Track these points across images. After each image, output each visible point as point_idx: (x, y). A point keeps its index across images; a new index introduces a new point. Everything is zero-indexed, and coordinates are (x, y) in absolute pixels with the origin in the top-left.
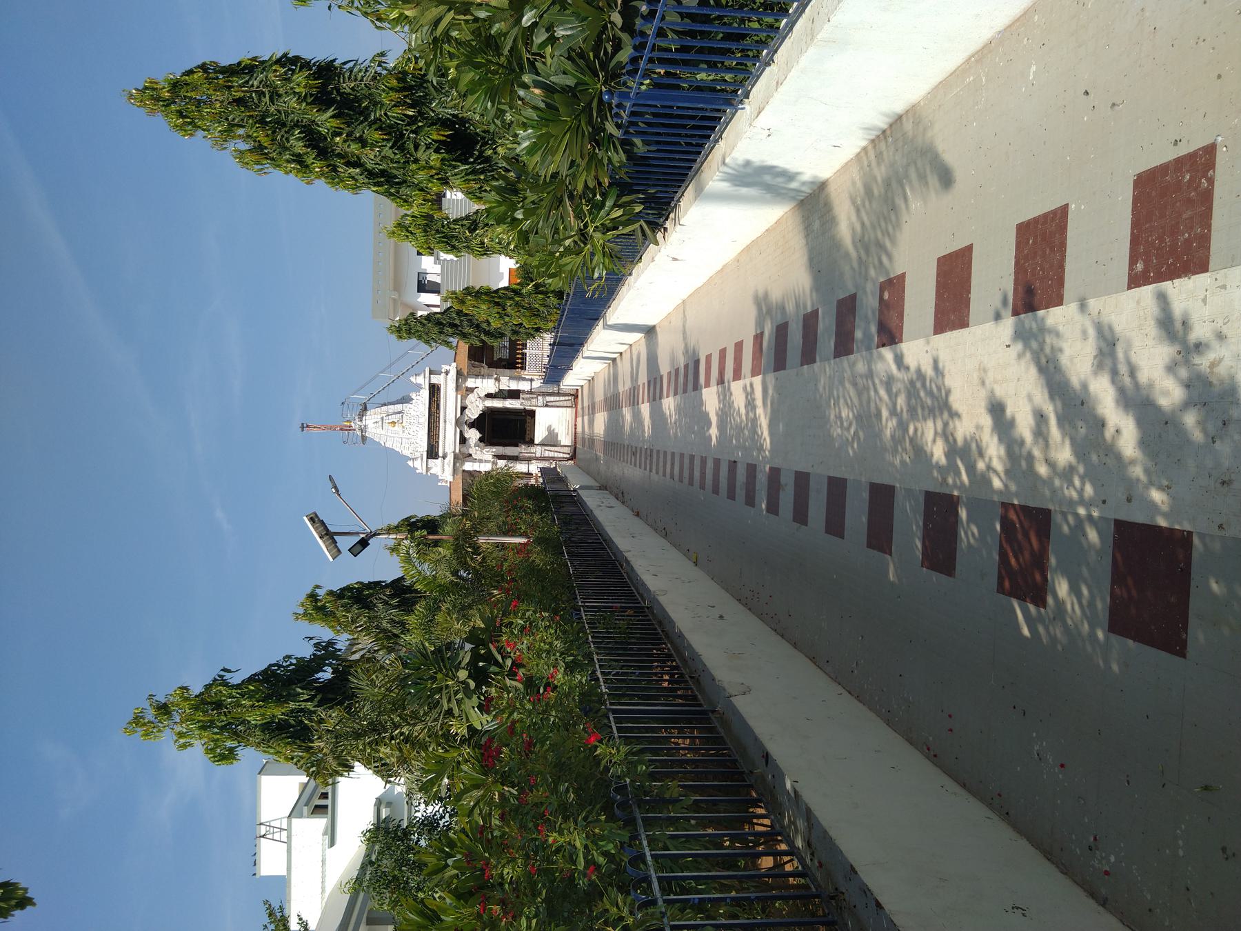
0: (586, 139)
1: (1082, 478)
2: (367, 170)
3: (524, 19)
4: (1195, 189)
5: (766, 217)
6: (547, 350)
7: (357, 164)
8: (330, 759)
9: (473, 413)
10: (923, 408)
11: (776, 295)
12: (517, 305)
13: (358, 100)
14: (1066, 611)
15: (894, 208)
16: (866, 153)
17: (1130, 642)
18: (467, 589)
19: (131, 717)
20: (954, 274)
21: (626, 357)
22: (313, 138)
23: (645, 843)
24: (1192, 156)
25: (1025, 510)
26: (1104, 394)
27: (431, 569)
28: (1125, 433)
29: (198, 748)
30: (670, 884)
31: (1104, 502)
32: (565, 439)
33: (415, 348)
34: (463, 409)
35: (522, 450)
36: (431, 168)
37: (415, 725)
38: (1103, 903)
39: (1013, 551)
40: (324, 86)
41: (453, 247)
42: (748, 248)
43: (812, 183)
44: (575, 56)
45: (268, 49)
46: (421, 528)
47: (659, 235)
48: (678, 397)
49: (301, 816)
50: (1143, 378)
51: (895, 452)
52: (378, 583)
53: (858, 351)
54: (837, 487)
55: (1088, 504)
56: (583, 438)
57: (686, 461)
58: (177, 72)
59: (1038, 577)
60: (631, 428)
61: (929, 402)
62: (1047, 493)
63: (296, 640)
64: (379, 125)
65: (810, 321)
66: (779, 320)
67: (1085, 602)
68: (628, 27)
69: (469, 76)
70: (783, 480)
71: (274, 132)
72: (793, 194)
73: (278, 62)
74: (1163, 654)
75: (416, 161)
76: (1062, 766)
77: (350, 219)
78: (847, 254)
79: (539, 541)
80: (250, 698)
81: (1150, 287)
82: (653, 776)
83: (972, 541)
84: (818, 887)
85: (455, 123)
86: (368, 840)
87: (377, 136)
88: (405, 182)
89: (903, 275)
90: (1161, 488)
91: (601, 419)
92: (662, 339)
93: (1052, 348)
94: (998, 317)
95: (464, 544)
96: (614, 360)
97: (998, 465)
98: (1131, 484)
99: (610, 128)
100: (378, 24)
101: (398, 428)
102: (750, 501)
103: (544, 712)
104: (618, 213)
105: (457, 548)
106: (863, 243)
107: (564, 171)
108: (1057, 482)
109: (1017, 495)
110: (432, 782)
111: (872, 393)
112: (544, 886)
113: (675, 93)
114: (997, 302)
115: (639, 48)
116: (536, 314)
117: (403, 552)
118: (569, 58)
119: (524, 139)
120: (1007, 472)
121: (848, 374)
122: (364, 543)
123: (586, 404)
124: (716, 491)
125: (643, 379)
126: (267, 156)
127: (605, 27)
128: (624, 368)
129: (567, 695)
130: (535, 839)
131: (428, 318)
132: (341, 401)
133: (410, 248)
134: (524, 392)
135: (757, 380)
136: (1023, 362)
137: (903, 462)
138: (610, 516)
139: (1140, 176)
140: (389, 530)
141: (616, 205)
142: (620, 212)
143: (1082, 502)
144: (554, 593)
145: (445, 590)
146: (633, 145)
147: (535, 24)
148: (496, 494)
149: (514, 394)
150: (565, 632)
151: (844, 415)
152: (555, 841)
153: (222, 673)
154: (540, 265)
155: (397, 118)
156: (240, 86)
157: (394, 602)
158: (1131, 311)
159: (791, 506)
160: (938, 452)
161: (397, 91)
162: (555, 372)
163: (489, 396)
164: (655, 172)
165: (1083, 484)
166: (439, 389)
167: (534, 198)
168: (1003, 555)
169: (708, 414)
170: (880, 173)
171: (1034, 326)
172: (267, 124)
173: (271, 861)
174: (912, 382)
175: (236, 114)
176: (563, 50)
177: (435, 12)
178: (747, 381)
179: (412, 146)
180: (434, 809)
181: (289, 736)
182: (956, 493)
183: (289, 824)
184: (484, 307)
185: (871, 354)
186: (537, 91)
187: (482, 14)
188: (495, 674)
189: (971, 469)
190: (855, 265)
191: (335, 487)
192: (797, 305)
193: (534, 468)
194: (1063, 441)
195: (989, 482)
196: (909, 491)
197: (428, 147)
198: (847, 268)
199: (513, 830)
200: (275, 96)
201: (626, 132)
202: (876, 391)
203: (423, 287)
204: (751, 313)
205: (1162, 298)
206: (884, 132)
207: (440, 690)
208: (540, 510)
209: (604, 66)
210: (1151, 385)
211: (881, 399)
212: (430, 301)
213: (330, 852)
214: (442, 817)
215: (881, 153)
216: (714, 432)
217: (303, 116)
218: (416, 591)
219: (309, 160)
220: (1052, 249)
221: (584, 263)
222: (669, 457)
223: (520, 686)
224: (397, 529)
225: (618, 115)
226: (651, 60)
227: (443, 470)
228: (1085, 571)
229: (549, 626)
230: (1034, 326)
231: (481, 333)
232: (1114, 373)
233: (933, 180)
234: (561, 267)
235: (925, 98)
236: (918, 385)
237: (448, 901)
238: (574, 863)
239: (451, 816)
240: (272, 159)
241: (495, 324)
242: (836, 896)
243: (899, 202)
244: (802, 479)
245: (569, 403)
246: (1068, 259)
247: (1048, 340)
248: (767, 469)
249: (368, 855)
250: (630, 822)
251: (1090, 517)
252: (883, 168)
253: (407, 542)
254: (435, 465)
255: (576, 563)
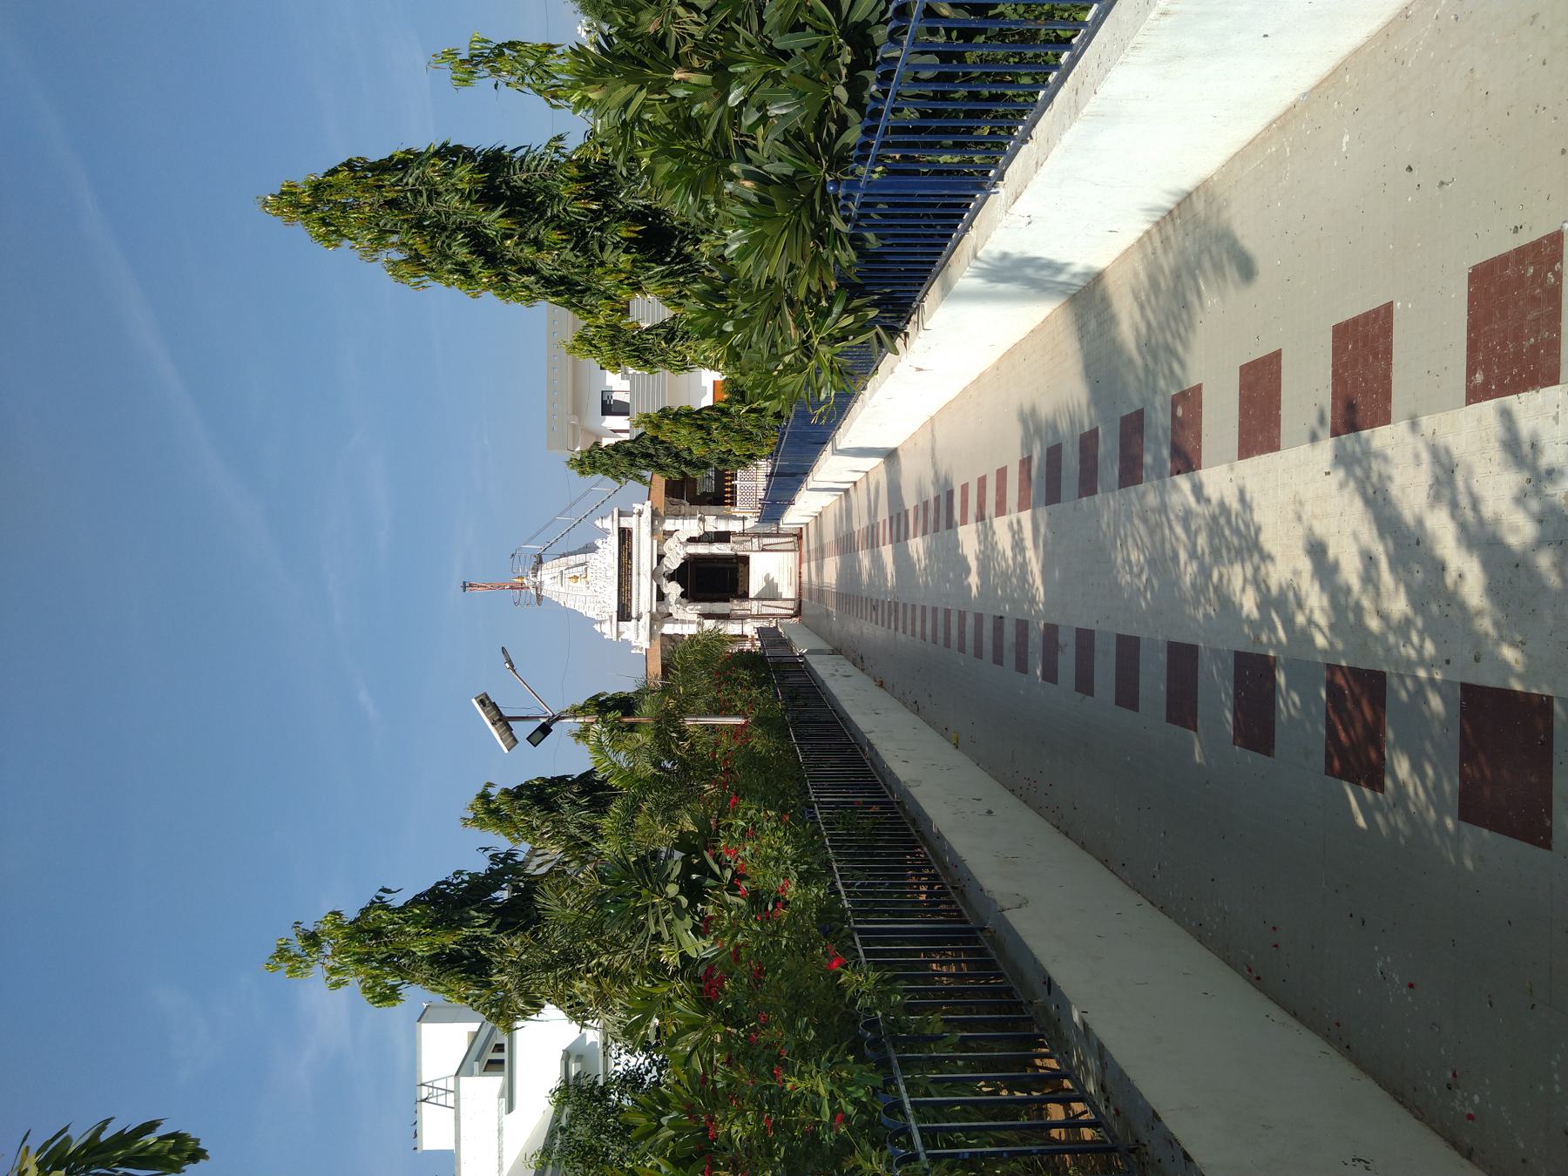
0: (808, 237)
1: (1421, 634)
2: (543, 277)
3: (731, 97)
4: (1541, 286)
5: (1032, 315)
6: (762, 483)
7: (532, 270)
8: (515, 995)
9: (673, 562)
10: (1229, 550)
11: (1045, 411)
12: (725, 427)
13: (531, 194)
14: (1407, 795)
15: (1185, 306)
16: (1150, 238)
17: (1485, 832)
18: (673, 784)
19: (275, 950)
20: (1261, 386)
21: (862, 486)
22: (481, 244)
23: (903, 1088)
24: (1536, 245)
25: (1355, 673)
26: (1442, 530)
27: (626, 759)
28: (1469, 578)
29: (354, 983)
30: (934, 1140)
31: (1448, 662)
32: (788, 591)
33: (601, 484)
34: (661, 557)
35: (735, 606)
36: (620, 271)
37: (615, 953)
38: (1469, 1155)
39: (1342, 723)
40: (491, 179)
41: (647, 362)
42: (1010, 352)
43: (1085, 274)
44: (792, 138)
45: (423, 139)
46: (614, 708)
47: (899, 342)
48: (927, 537)
49: (471, 1074)
50: (1488, 510)
51: (1197, 603)
52: (562, 779)
53: (1149, 480)
54: (1128, 647)
55: (1429, 666)
56: (810, 590)
57: (941, 617)
58: (318, 171)
59: (1373, 755)
60: (870, 576)
61: (1236, 541)
62: (1381, 652)
63: (469, 852)
64: (558, 223)
65: (1088, 442)
66: (1051, 442)
67: (1430, 784)
68: (855, 102)
69: (666, 167)
70: (1062, 639)
71: (433, 238)
72: (1062, 288)
73: (437, 154)
74: (1526, 846)
75: (602, 264)
76: (1411, 986)
77: (525, 334)
78: (1131, 361)
79: (759, 722)
80: (416, 923)
81: (1492, 402)
82: (909, 1009)
83: (1293, 711)
84: (1114, 1138)
85: (647, 216)
86: (558, 1101)
87: (555, 236)
88: (589, 289)
89: (1199, 387)
90: (1513, 644)
91: (832, 566)
92: (906, 463)
93: (1380, 476)
94: (1314, 438)
95: (667, 726)
96: (846, 491)
97: (1321, 619)
98: (1478, 639)
99: (837, 222)
100: (554, 102)
101: (581, 584)
102: (1022, 666)
103: (775, 933)
104: (848, 321)
105: (660, 734)
106: (1149, 347)
107: (782, 275)
108: (1391, 639)
109: (1344, 654)
110: (638, 1025)
111: (1167, 531)
112: (781, 1144)
113: (910, 180)
114: (1313, 420)
115: (869, 131)
116: (748, 437)
117: (592, 739)
118: (785, 142)
119: (733, 241)
120: (1332, 627)
121: (1136, 508)
122: (545, 730)
123: (812, 546)
124: (978, 653)
125: (883, 515)
126: (425, 267)
127: (827, 103)
128: (860, 500)
129: (802, 912)
130: (769, 1087)
131: (616, 447)
132: (511, 555)
133: (593, 363)
134: (735, 534)
135: (1026, 516)
136: (1346, 492)
137: (1206, 616)
138: (846, 687)
139: (1475, 269)
140: (575, 712)
141: (845, 311)
142: (850, 320)
143: (1421, 662)
144: (781, 786)
145: (646, 785)
146: (864, 240)
147: (744, 102)
148: (704, 664)
149: (723, 537)
150: (796, 835)
151: (1133, 557)
152: (794, 1088)
153: (381, 894)
154: (755, 386)
155: (579, 214)
156: (393, 185)
157: (583, 801)
158: (1471, 430)
159: (1072, 672)
160: (1249, 603)
161: (578, 181)
162: (773, 507)
163: (692, 540)
164: (890, 282)
165: (1422, 640)
166: (630, 533)
167: (746, 305)
168: (1330, 728)
169: (965, 558)
170: (1167, 262)
171: (1358, 449)
172: (424, 227)
173: (435, 1132)
174: (1214, 518)
175: (389, 219)
176: (778, 133)
177: (624, 92)
178: (1014, 517)
179: (596, 247)
180: (638, 1061)
181: (464, 970)
182: (1271, 654)
183: (457, 1084)
184: (684, 432)
185: (1164, 484)
186: (748, 184)
187: (680, 93)
188: (713, 888)
189: (1289, 623)
190: (1141, 374)
191: (510, 662)
192: (1072, 422)
193: (750, 629)
194: (1397, 589)
195: (1311, 641)
196: (1216, 652)
197: (616, 246)
198: (1131, 380)
199: (742, 1074)
200: (433, 194)
201: (856, 226)
202: (1171, 528)
203: (609, 408)
204: (1015, 434)
205: (1506, 415)
206: (1170, 212)
207: (645, 909)
208: (759, 682)
209: (827, 148)
210: (1497, 520)
211: (1177, 539)
212: (617, 428)
213: (508, 1118)
214: (648, 1071)
215: (1168, 238)
216: (973, 580)
217: (467, 217)
218: (610, 788)
219: (475, 270)
220: (1376, 356)
221: (808, 383)
222: (918, 613)
223: (742, 902)
224: (581, 710)
225: (845, 207)
226: (884, 145)
227: (637, 635)
228: (1428, 746)
229: (777, 828)
230: (1358, 449)
231: (683, 465)
232: (1454, 506)
233: (1232, 272)
234: (780, 388)
235: (1219, 171)
236: (1222, 521)
237: (664, 1169)
238: (818, 1113)
239: (659, 1070)
240: (432, 270)
241: (698, 451)
242: (1136, 1149)
243: (1192, 297)
244: (1085, 639)
245: (790, 546)
246: (1394, 368)
247: (1375, 466)
248: (1042, 626)
249: (556, 1119)
250: (884, 1064)
251: (1432, 680)
252: (1171, 256)
253: (597, 727)
254: (628, 628)
255: (806, 748)
